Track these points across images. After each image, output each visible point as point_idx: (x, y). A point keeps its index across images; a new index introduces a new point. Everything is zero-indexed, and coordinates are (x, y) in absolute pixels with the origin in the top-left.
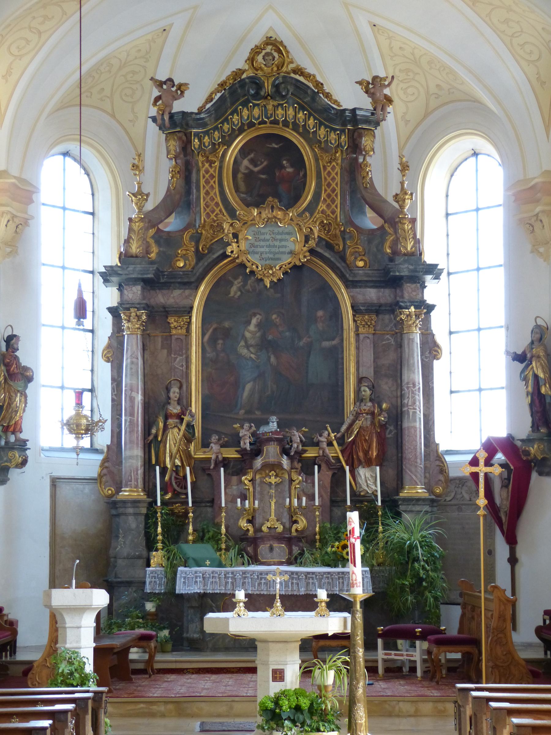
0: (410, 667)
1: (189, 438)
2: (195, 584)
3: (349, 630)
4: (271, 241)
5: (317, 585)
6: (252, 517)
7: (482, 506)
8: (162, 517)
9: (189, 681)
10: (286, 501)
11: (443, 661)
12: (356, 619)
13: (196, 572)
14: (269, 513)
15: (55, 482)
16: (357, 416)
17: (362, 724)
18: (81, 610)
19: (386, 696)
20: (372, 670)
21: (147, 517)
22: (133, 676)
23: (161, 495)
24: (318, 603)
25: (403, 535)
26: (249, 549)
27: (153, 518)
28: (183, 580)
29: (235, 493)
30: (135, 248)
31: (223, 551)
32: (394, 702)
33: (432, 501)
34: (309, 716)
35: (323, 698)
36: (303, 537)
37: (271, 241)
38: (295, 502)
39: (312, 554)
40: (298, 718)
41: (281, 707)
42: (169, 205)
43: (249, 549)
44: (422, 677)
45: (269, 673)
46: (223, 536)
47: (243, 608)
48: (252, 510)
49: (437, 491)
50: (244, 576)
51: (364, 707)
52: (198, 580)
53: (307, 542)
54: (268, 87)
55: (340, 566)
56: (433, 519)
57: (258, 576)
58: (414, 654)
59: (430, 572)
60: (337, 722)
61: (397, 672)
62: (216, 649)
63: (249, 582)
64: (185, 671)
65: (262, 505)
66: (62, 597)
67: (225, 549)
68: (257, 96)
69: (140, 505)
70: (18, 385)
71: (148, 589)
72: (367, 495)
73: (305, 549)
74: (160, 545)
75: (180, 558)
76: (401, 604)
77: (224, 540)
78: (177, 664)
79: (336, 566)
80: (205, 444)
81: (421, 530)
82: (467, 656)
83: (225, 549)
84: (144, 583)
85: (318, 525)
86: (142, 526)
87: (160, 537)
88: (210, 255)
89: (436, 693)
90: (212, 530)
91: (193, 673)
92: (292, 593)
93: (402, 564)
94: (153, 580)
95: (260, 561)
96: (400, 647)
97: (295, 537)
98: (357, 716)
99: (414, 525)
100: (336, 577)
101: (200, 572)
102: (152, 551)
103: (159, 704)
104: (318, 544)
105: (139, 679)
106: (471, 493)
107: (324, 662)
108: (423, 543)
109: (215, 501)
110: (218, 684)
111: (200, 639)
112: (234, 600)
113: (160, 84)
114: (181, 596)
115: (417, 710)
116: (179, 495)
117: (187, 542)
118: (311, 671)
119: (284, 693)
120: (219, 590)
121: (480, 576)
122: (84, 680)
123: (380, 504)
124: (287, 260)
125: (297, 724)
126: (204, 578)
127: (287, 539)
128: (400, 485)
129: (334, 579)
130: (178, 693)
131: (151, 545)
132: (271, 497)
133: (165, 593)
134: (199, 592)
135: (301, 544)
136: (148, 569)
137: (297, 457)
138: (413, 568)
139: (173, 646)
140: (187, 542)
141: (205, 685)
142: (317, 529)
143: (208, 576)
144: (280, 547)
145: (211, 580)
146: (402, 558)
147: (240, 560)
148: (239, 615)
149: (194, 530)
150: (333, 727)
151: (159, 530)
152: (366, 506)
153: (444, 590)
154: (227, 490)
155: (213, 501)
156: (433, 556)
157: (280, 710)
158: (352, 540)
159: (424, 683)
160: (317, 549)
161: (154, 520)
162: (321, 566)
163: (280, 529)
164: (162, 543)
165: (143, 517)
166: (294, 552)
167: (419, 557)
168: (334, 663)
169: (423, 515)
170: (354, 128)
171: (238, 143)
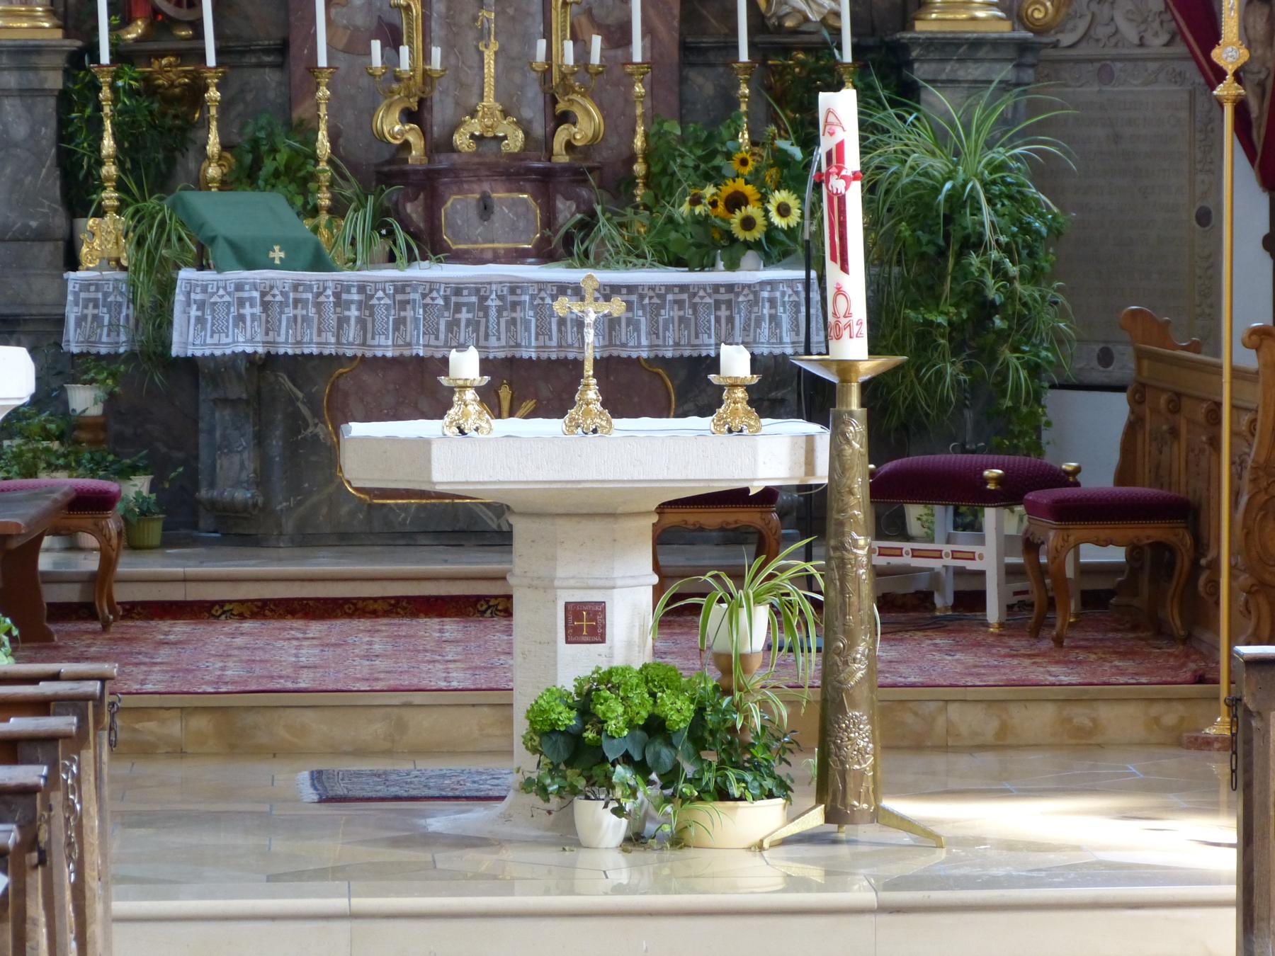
0: (957, 594)
2: (236, 325)
3: (821, 476)
5: (643, 327)
6: (421, 102)
7: (1230, 69)
8: (115, 101)
9: (239, 641)
10: (534, 47)
11: (1070, 572)
12: (848, 442)
13: (239, 287)
14: (476, 90)
17: (862, 773)
19: (906, 686)
21: (64, 100)
22: (53, 627)
23: (112, 29)
24: (720, 389)
25: (928, 161)
26: (409, 208)
27: (85, 106)
28: (194, 312)
29: (360, 20)
31: (324, 217)
32: (932, 706)
33: (1023, 47)
34: (692, 751)
35: (737, 695)
36: (591, 170)
38: (568, 53)
39: (621, 225)
40: (657, 756)
41: (600, 723)
43: (409, 208)
44: (1001, 625)
45: (555, 616)
46: (323, 165)
47: (474, 408)
48: (419, 78)
49: (1037, 15)
50: (399, 297)
51: (871, 721)
52: (247, 311)
53: (601, 186)
55: (721, 264)
56: (1022, 109)
57: (446, 299)
58: (977, 549)
59: (1017, 285)
60: (780, 770)
61: (915, 608)
63: (416, 320)
64: (217, 610)
65: (453, 60)
67: (330, 211)
69: (43, 61)
71: (74, 342)
72: (805, 28)
73: (599, 209)
74: (110, 196)
75: (180, 239)
76: (918, 388)
77: (324, 179)
78: (189, 585)
79: (706, 264)
81: (989, 145)
82: (1152, 563)
83: (330, 211)
84: (60, 321)
85: (640, 129)
86: (48, 132)
87: (109, 170)
89: (1063, 675)
90: (287, 146)
91: (242, 617)
92: (562, 355)
93: (922, 256)
94: (90, 311)
95: (448, 249)
96: (914, 527)
97: (565, 169)
98: (849, 750)
99: (967, 127)
100: (708, 300)
101: (254, 286)
102: (86, 216)
103: (167, 714)
104: (640, 192)
105: (69, 634)
106: (1145, 21)
107: (738, 577)
108: (995, 190)
109: (293, 50)
110: (339, 651)
111: (255, 505)
112: (444, 380)
114: (190, 363)
115: (1004, 730)
117: (201, 184)
118: (696, 609)
119: (608, 680)
123: (847, 57)
125: (654, 776)
126: (266, 306)
127: (545, 181)
129: (700, 309)
130: (220, 680)
131: (78, 197)
132: (482, 35)
133: (131, 356)
134: (249, 350)
135: (584, 193)
136: (71, 275)
138: (962, 270)
139: (164, 529)
140: (201, 184)
141: (298, 652)
142: (639, 142)
143: (279, 298)
144: (514, 204)
145: (290, 311)
146: (925, 238)
147: (380, 246)
148: (462, 432)
149: (225, 146)
150: (769, 783)
151: (108, 145)
152: (802, 64)
153: (1061, 342)
154: (333, 11)
156: (1026, 229)
157: (599, 733)
158: (837, 184)
159: (1012, 642)
160: (636, 207)
161: (88, 111)
162: (652, 266)
163: (515, 141)
164: (117, 189)
165: (52, 102)
166: (561, 219)
167: (981, 235)
168: (768, 584)
169: (994, 98)
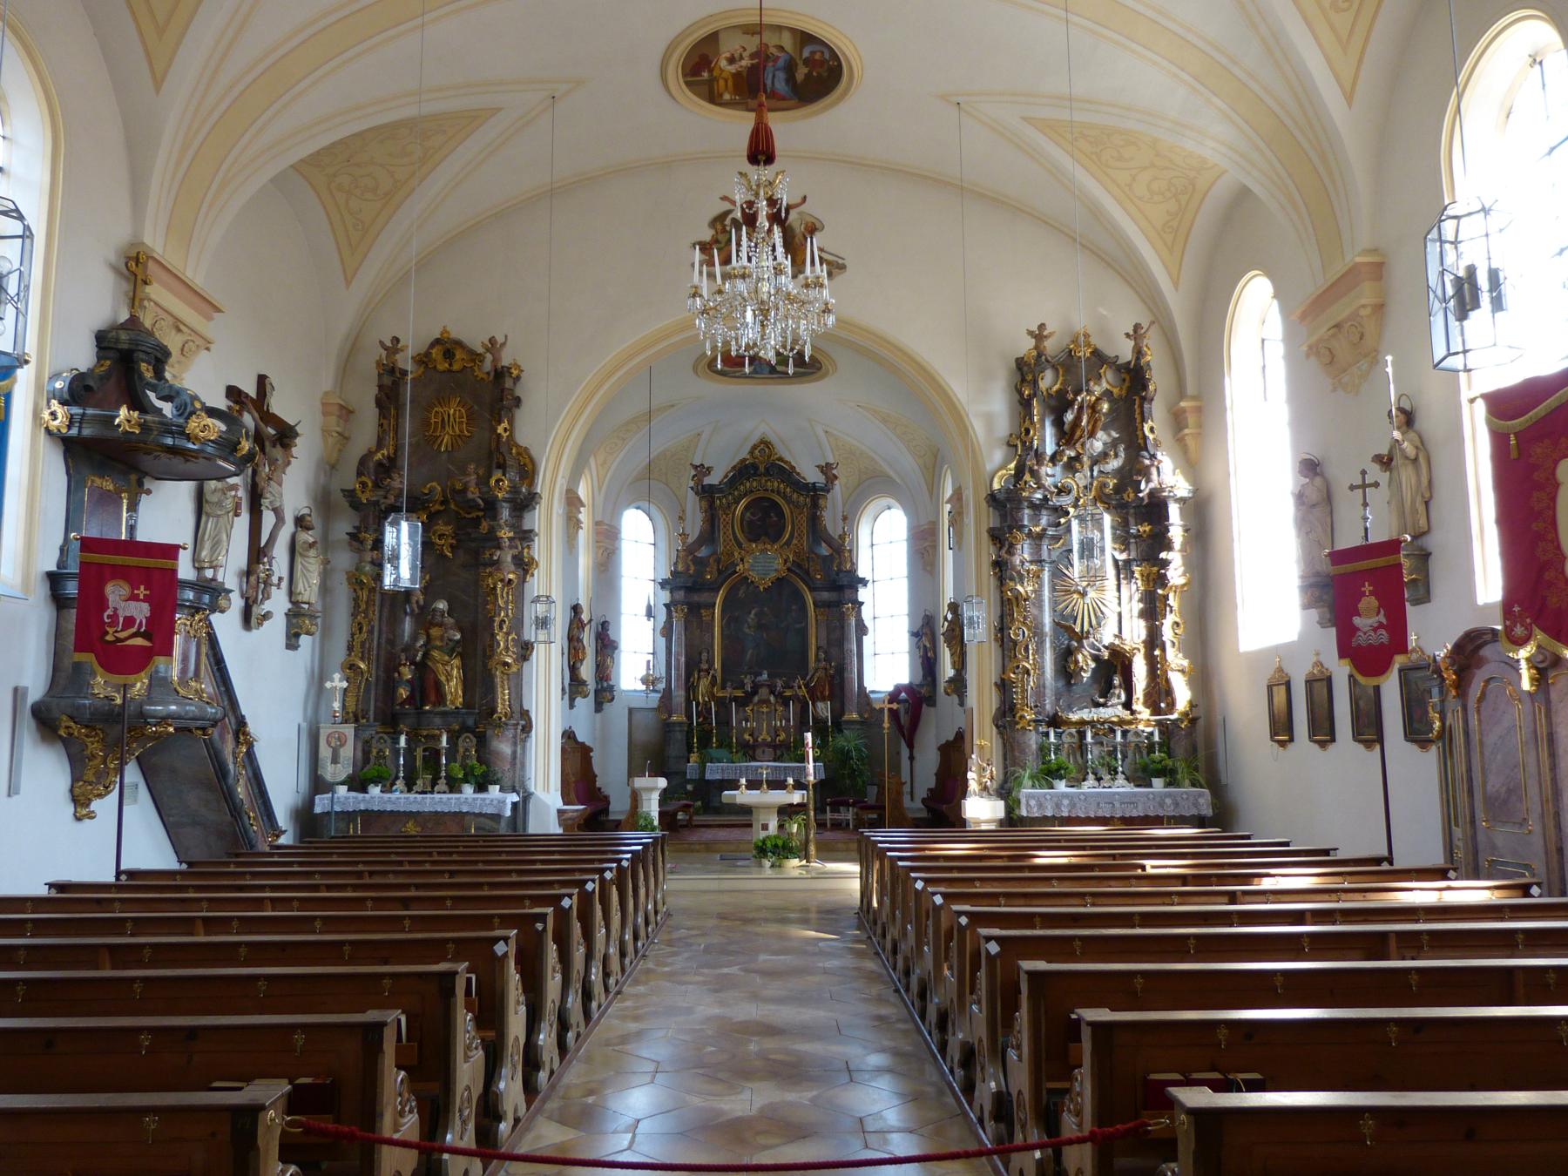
1: (713, 683)
4: (763, 564)
15: (631, 711)
16: (816, 670)
18: (651, 790)
30: (680, 568)
37: (763, 564)
42: (701, 541)
54: (762, 469)
62: (730, 813)
66: (640, 782)
68: (755, 474)
70: (609, 651)
80: (723, 687)
88: (727, 570)
113: (696, 467)
116: (707, 718)
120: (732, 777)
122: (653, 829)
124: (773, 575)
127: (774, 746)
128: (843, 714)
131: (690, 750)
137: (779, 696)
141: (722, 834)
155: (729, 722)
170: (814, 495)
171: (743, 503)
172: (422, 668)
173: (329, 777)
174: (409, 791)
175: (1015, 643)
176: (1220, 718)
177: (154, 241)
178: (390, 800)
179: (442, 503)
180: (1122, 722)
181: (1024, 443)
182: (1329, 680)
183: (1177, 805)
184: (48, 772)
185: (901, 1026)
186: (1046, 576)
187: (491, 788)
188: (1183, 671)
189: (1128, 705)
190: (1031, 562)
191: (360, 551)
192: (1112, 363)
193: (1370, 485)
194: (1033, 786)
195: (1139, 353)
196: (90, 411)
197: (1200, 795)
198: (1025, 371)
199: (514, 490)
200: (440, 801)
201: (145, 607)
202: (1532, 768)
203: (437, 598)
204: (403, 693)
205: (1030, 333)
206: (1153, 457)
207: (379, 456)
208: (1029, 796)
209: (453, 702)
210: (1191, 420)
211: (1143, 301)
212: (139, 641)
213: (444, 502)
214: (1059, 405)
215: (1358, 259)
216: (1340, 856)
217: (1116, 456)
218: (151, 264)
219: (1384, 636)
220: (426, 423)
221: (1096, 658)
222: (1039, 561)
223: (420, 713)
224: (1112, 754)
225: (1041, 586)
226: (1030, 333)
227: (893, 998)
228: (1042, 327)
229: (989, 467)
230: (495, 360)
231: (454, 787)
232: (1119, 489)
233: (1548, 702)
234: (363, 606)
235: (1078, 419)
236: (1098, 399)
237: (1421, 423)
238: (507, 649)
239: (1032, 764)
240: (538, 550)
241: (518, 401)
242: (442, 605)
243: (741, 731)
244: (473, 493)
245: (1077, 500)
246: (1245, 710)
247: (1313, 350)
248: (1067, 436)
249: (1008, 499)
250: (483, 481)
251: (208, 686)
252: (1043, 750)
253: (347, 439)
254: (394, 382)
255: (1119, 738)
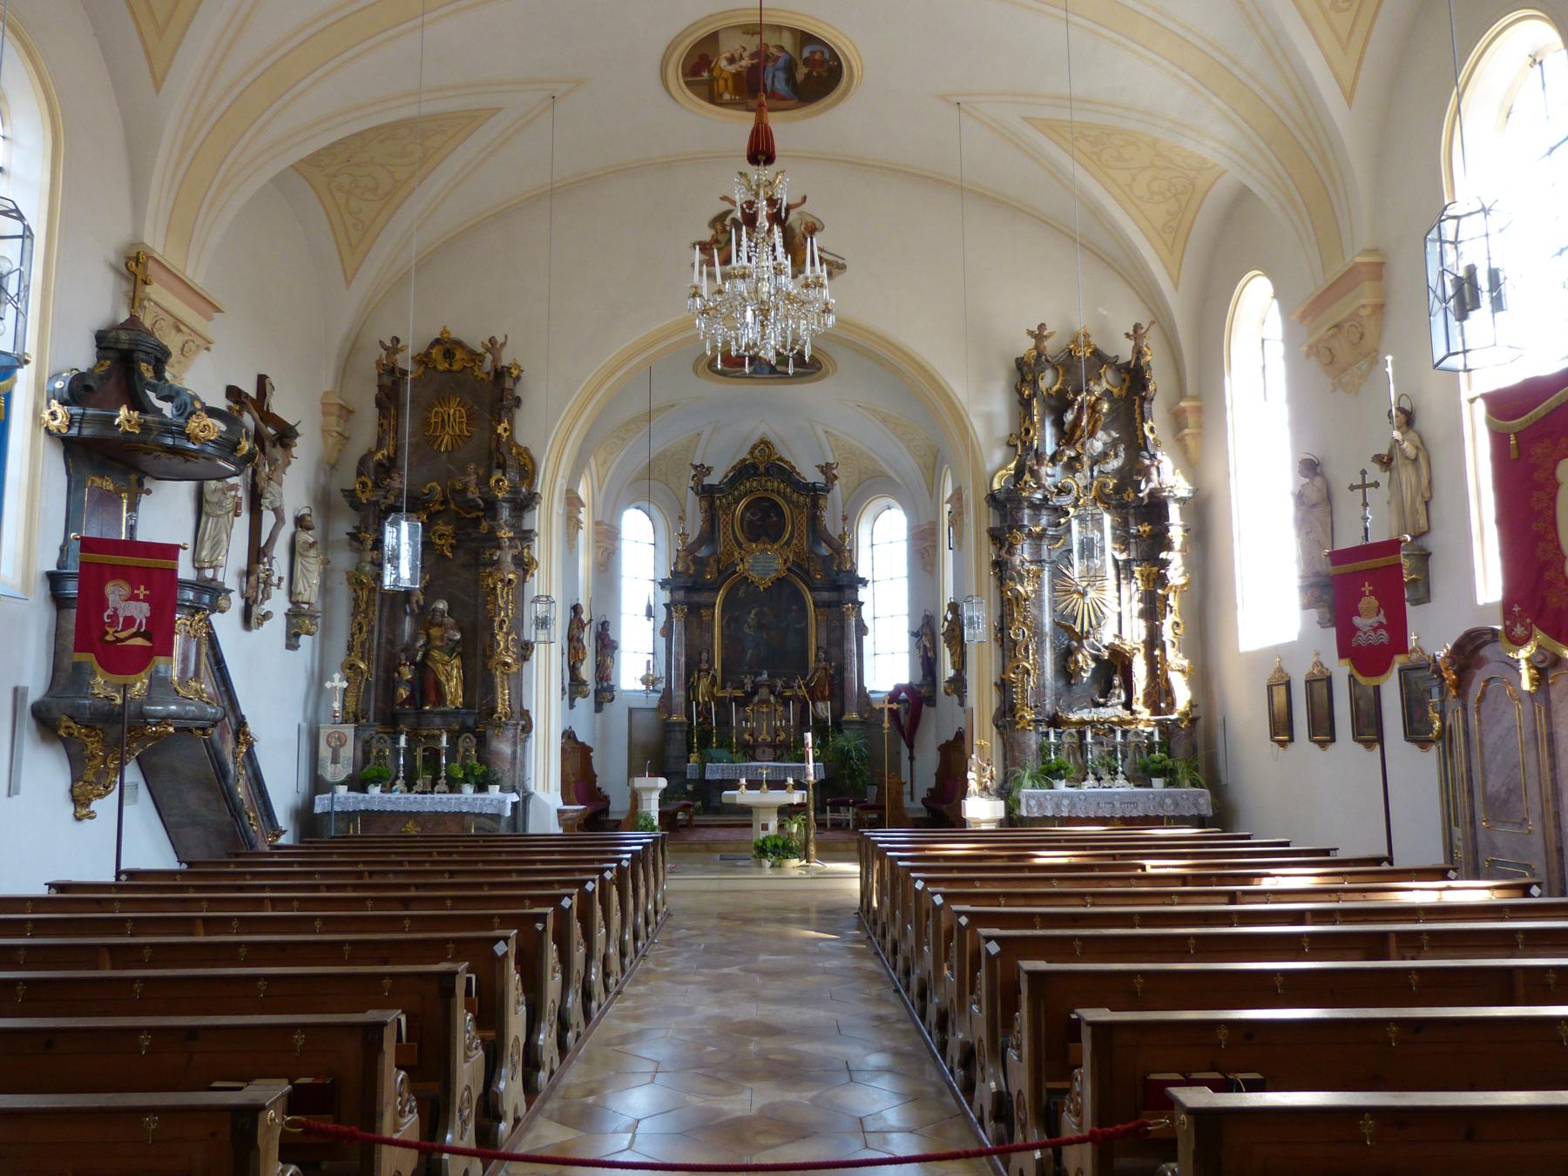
1: (713, 683)
4: (763, 564)
15: (631, 711)
16: (816, 670)
18: (651, 790)
20: (821, 825)
30: (680, 568)
37: (763, 564)
42: (701, 541)
54: (762, 469)
62: (730, 813)
66: (640, 782)
68: (755, 474)
70: (609, 651)
80: (723, 687)
88: (727, 570)
113: (696, 467)
116: (707, 718)
120: (732, 777)
121: (262, 1011)
122: (653, 829)
124: (773, 575)
127: (774, 746)
128: (843, 714)
131: (690, 750)
137: (779, 696)
141: (722, 834)
155: (729, 722)
170: (814, 495)
171: (743, 503)
172: (422, 668)
173: (329, 777)
174: (409, 791)
175: (1015, 643)
176: (1220, 718)
177: (154, 241)
178: (390, 800)
179: (442, 503)
180: (1122, 722)
181: (1024, 443)
182: (1329, 680)
183: (1177, 805)
184: (48, 772)
185: (901, 1026)
186: (1046, 576)
187: (491, 788)
188: (1183, 671)
189: (1128, 705)
190: (1031, 562)
191: (360, 551)
192: (1112, 363)
193: (1370, 485)
194: (1033, 786)
195: (1139, 353)
196: (90, 411)
197: (1200, 795)
198: (1025, 371)
199: (514, 490)
200: (440, 801)
201: (145, 607)
202: (1532, 768)
203: (437, 598)
204: (403, 693)
205: (1030, 333)
206: (1153, 457)
207: (379, 456)
208: (1029, 796)
209: (453, 702)
210: (1191, 420)
211: (1143, 301)
212: (139, 641)
213: (444, 502)
214: (1059, 405)
215: (1358, 259)
216: (1340, 856)
217: (1116, 456)
218: (151, 264)
219: (1384, 636)
220: (426, 423)
221: (1096, 658)
222: (1039, 561)
223: (420, 713)
224: (1112, 754)
225: (1041, 586)
226: (1030, 333)
227: (893, 998)
228: (1042, 327)
229: (989, 467)
230: (495, 360)
231: (454, 787)
232: (1119, 489)
233: (1548, 702)
234: (363, 606)
235: (1078, 419)
236: (1098, 399)
237: (1421, 423)
238: (507, 649)
239: (1032, 764)
240: (538, 550)
241: (518, 401)
242: (442, 605)
243: (741, 731)
244: (473, 493)
245: (1077, 500)
246: (1245, 710)
247: (1313, 350)
248: (1067, 436)
249: (1008, 499)
250: (483, 481)
251: (208, 686)
252: (1043, 750)
253: (347, 439)
254: (394, 382)
255: (1119, 738)
